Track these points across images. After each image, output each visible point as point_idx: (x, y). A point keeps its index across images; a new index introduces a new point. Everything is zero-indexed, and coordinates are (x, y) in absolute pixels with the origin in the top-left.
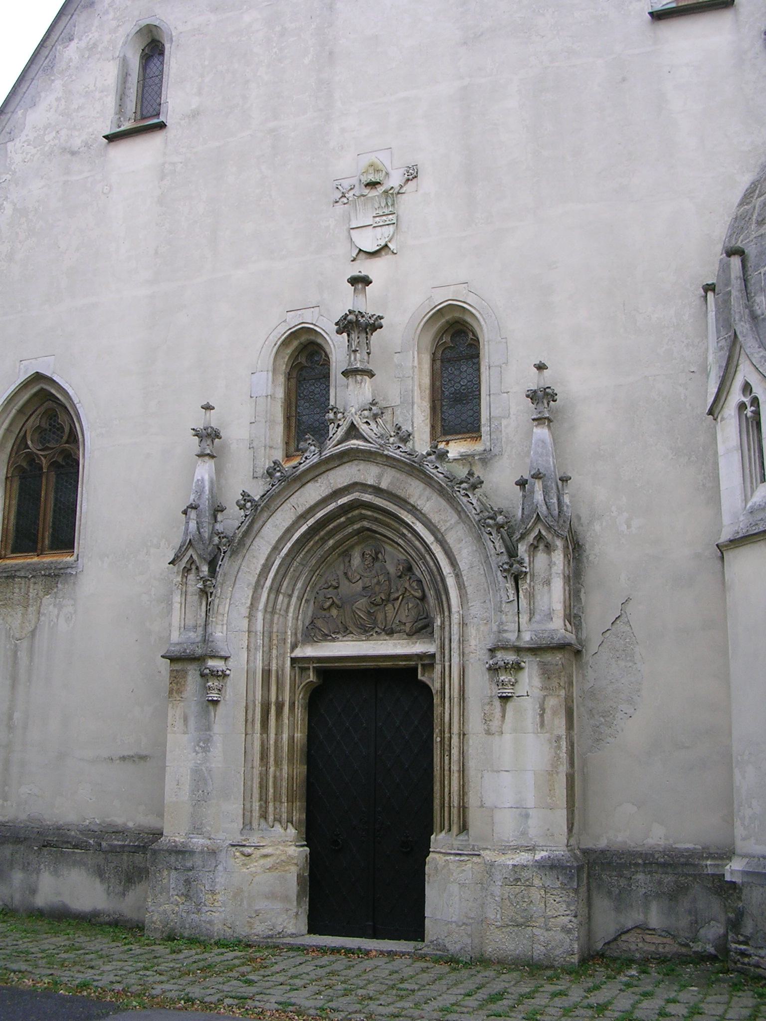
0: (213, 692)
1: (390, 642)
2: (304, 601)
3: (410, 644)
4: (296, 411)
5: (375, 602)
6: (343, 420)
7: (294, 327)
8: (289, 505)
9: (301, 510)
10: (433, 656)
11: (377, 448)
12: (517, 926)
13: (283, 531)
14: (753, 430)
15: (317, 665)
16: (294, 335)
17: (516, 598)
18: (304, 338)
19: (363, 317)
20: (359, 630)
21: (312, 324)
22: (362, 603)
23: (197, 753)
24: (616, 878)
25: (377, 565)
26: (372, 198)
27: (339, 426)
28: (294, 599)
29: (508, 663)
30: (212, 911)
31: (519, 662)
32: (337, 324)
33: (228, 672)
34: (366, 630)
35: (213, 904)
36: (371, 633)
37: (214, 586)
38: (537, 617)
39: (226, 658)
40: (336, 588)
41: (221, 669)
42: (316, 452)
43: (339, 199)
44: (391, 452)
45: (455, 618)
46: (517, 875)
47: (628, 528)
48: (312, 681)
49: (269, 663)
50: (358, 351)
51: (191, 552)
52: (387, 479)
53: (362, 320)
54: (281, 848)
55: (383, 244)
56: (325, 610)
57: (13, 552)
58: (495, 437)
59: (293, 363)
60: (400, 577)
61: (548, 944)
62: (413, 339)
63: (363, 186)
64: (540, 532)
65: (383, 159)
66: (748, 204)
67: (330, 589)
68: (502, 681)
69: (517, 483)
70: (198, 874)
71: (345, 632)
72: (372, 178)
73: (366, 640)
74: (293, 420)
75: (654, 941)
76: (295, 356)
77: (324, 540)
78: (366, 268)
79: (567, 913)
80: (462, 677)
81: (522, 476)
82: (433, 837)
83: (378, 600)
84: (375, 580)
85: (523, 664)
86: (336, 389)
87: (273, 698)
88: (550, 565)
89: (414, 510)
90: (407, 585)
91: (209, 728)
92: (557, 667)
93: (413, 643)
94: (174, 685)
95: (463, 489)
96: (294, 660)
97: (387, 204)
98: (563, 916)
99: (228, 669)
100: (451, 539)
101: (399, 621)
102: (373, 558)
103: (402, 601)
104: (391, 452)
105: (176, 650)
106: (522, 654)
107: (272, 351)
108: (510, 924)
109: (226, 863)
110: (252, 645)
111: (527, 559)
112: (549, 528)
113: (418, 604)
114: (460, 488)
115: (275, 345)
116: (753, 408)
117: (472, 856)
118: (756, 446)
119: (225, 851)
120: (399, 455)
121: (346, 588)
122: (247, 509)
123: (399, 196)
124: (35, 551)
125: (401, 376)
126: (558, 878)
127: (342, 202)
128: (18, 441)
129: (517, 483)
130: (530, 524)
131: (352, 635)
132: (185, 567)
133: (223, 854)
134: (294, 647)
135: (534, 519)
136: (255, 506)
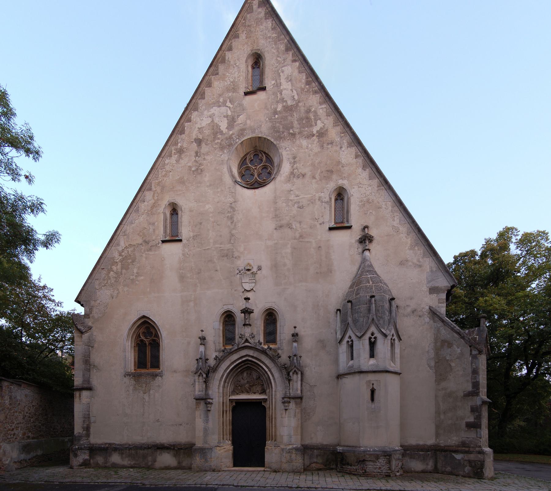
10: (267, 399)
18: (228, 313)
22: (247, 385)
25: (251, 376)
26: (249, 274)
32: (241, 311)
34: (248, 392)
38: (294, 390)
39: (212, 399)
45: (274, 390)
46: (289, 452)
52: (256, 354)
53: (249, 310)
57: (138, 368)
60: (257, 379)
65: (251, 262)
66: (352, 288)
69: (288, 357)
72: (249, 268)
74: (225, 336)
76: (225, 318)
77: (237, 369)
78: (249, 295)
82: (267, 442)
91: (208, 417)
96: (229, 400)
100: (272, 370)
105: (197, 397)
111: (292, 376)
112: (298, 369)
121: (242, 382)
124: (146, 368)
128: (137, 336)
129: (288, 357)
133: (213, 449)
134: (229, 396)
136: (219, 359)
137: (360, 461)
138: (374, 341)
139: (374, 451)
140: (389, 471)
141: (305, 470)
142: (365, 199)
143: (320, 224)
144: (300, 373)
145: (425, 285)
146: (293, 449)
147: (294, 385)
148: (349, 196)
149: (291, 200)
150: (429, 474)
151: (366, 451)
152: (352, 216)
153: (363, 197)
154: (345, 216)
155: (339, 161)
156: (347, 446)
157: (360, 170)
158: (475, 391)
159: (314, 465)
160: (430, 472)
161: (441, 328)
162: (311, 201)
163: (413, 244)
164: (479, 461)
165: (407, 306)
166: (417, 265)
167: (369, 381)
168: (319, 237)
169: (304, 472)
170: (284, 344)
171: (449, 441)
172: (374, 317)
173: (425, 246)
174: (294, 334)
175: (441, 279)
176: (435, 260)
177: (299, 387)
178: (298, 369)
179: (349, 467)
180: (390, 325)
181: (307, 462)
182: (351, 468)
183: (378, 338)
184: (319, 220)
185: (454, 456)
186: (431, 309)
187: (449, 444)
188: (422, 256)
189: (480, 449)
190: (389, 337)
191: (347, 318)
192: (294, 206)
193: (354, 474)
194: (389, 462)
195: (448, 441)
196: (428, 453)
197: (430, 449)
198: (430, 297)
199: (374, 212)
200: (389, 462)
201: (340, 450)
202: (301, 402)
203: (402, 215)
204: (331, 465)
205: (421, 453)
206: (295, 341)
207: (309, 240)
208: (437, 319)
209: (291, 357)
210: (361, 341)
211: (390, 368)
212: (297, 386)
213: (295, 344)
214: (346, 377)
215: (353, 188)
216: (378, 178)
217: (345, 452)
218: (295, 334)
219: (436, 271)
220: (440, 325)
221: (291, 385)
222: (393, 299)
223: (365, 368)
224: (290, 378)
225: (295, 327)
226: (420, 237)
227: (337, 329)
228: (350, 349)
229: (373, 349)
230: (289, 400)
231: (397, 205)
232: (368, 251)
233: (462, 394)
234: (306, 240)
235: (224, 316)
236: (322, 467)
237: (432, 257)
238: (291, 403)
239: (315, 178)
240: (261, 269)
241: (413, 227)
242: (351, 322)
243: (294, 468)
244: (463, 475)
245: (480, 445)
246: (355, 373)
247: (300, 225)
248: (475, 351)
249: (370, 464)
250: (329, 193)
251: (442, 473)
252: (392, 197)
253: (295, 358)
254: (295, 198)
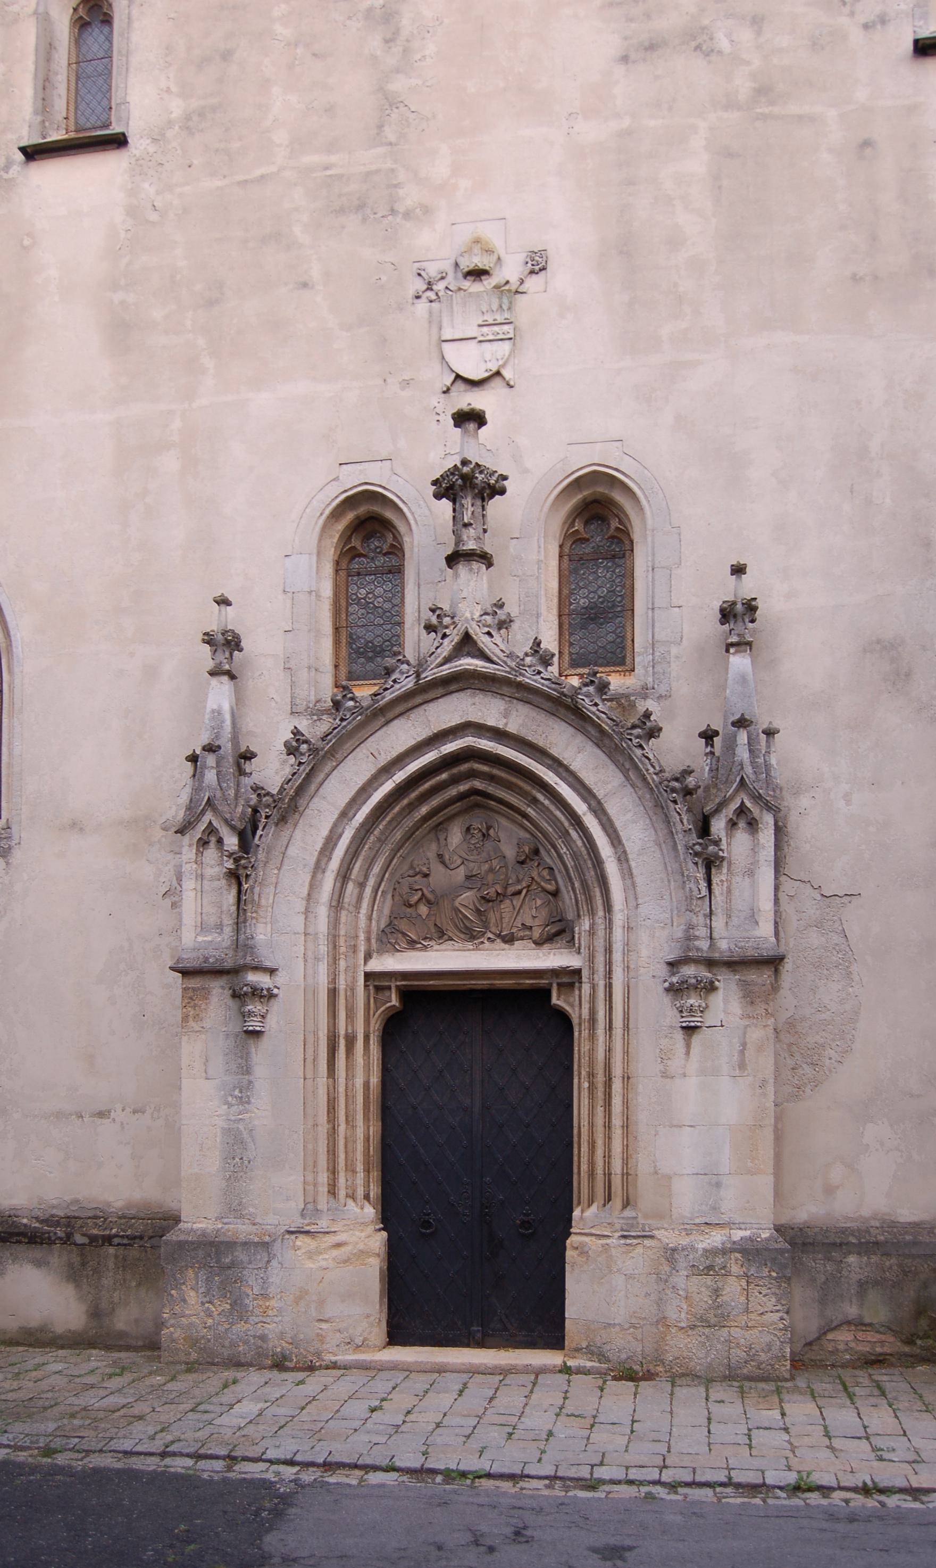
0: (255, 1019)
1: (511, 952)
2: (380, 893)
3: (541, 955)
4: (347, 620)
5: (488, 897)
6: (452, 627)
7: (351, 489)
8: (364, 751)
9: (384, 759)
10: (578, 972)
11: (506, 672)
13: (357, 789)
15: (403, 983)
16: (350, 502)
17: (708, 894)
18: (362, 510)
19: (481, 472)
20: (462, 936)
21: (380, 486)
22: (468, 897)
23: (230, 1105)
24: (822, 1262)
25: (489, 845)
26: (478, 295)
27: (444, 636)
28: (368, 891)
30: (265, 1323)
31: (713, 980)
32: (435, 483)
33: (275, 991)
34: (471, 935)
35: (265, 1313)
36: (482, 940)
37: (252, 867)
38: (735, 921)
39: (272, 971)
40: (426, 876)
41: (267, 987)
42: (410, 674)
43: (423, 292)
44: (528, 678)
45: (619, 918)
48: (394, 1006)
49: (335, 979)
50: (471, 524)
51: (209, 816)
54: (357, 1233)
55: (495, 369)
56: (410, 906)
58: (661, 671)
59: (342, 549)
62: (538, 520)
63: (460, 275)
64: (743, 802)
65: (492, 233)
67: (417, 878)
68: (691, 1006)
70: (240, 1272)
71: (440, 938)
72: (478, 261)
73: (473, 950)
75: (869, 1339)
77: (412, 807)
79: (777, 1308)
80: (626, 1000)
81: (709, 725)
83: (493, 894)
84: (486, 866)
85: (717, 983)
86: (419, 588)
87: (342, 1031)
89: (557, 765)
90: (535, 874)
91: (247, 1070)
92: (763, 988)
93: (544, 955)
94: (190, 1009)
95: (637, 737)
96: (368, 976)
97: (501, 307)
98: (772, 1312)
99: (275, 987)
101: (523, 924)
102: (484, 835)
103: (526, 895)
104: (529, 679)
105: (192, 960)
106: (715, 970)
107: (316, 523)
108: (699, 1324)
109: (282, 1257)
110: (310, 954)
113: (550, 900)
114: (631, 734)
115: (321, 514)
117: (642, 1239)
119: (280, 1240)
120: (540, 683)
121: (439, 876)
122: (302, 754)
123: (518, 296)
125: (520, 573)
126: (766, 1265)
127: (427, 298)
131: (453, 942)
132: (200, 839)
133: (277, 1245)
134: (368, 957)
136: (314, 751)
225: (738, 570)
235: (341, 526)
240: (544, 269)
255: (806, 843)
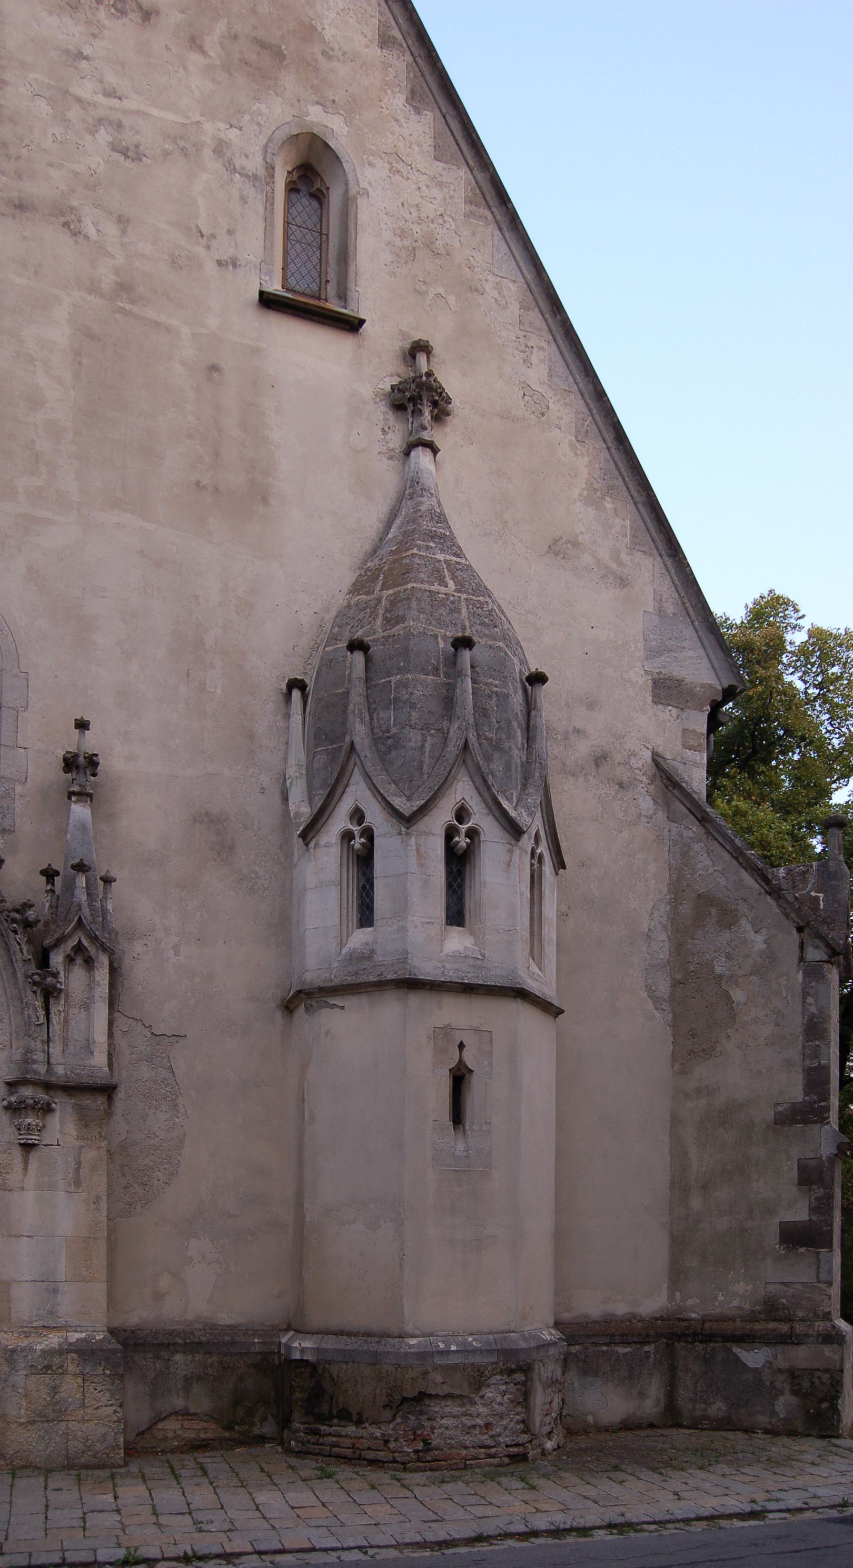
12: (48, 1421)
14: (353, 867)
29: (38, 1102)
31: (50, 1102)
47: (176, 955)
61: (87, 1440)
64: (80, 941)
66: (367, 594)
68: (29, 1125)
69: (43, 873)
79: (112, 1402)
85: (54, 1105)
88: (91, 985)
98: (106, 1406)
111: (62, 973)
112: (94, 939)
116: (363, 840)
118: (355, 886)
129: (43, 873)
130: (69, 929)
135: (74, 922)
137: (404, 1400)
138: (468, 845)
139: (466, 1351)
140: (524, 1438)
141: (131, 1451)
142: (416, 228)
143: (219, 263)
144: (104, 959)
145: (639, 664)
146: (68, 1351)
147: (73, 1023)
148: (352, 192)
149: (79, 100)
150: (649, 1432)
151: (432, 1354)
152: (361, 281)
153: (408, 216)
154: (332, 275)
155: (313, 28)
156: (340, 1333)
157: (398, 102)
158: (815, 1102)
159: (172, 1425)
160: (652, 1426)
161: (696, 847)
162: (181, 143)
163: (596, 486)
164: (827, 1371)
165: (577, 731)
166: (613, 573)
167: (446, 1032)
168: (213, 322)
169: (126, 1464)
170: (19, 805)
171: (721, 1298)
172: (471, 735)
173: (640, 506)
174: (76, 756)
175: (691, 653)
176: (673, 571)
177: (100, 1037)
178: (94, 939)
179: (351, 1429)
180: (531, 790)
181: (141, 1415)
182: (361, 1432)
183: (482, 838)
184: (214, 243)
185: (737, 1359)
186: (657, 760)
187: (718, 1311)
188: (627, 540)
189: (828, 1324)
190: (527, 842)
191: (344, 723)
192: (93, 132)
193: (373, 1462)
194: (524, 1398)
195: (716, 1298)
196: (646, 1348)
197: (652, 1333)
198: (655, 715)
199: (451, 299)
200: (526, 1400)
201: (303, 1350)
202: (109, 1113)
203: (557, 353)
204: (252, 1424)
205: (622, 1350)
206: (83, 795)
207: (162, 318)
208: (680, 808)
209: (57, 873)
210: (413, 840)
211: (529, 981)
212: (90, 1026)
213: (80, 811)
214: (334, 1006)
215: (371, 164)
216: (471, 170)
217: (329, 1362)
218: (81, 760)
219: (674, 614)
220: (691, 835)
221: (54, 1019)
222: (538, 679)
223: (427, 970)
224: (49, 980)
225: (82, 725)
226: (621, 465)
227: (292, 771)
228: (354, 871)
229: (461, 886)
230: (42, 1096)
231: (542, 303)
232: (428, 452)
233: (770, 1115)
234: (152, 314)
236: (210, 1435)
237: (661, 556)
238: (57, 1115)
239: (201, 50)
241: (598, 418)
242: (367, 741)
243: (76, 1446)
244: (769, 1427)
245: (826, 1310)
246: (381, 985)
247: (124, 232)
248: (817, 947)
249: (448, 1409)
250: (263, 140)
251: (695, 1425)
252: (522, 264)
253: (81, 881)
254: (100, 99)
255: (138, 985)
